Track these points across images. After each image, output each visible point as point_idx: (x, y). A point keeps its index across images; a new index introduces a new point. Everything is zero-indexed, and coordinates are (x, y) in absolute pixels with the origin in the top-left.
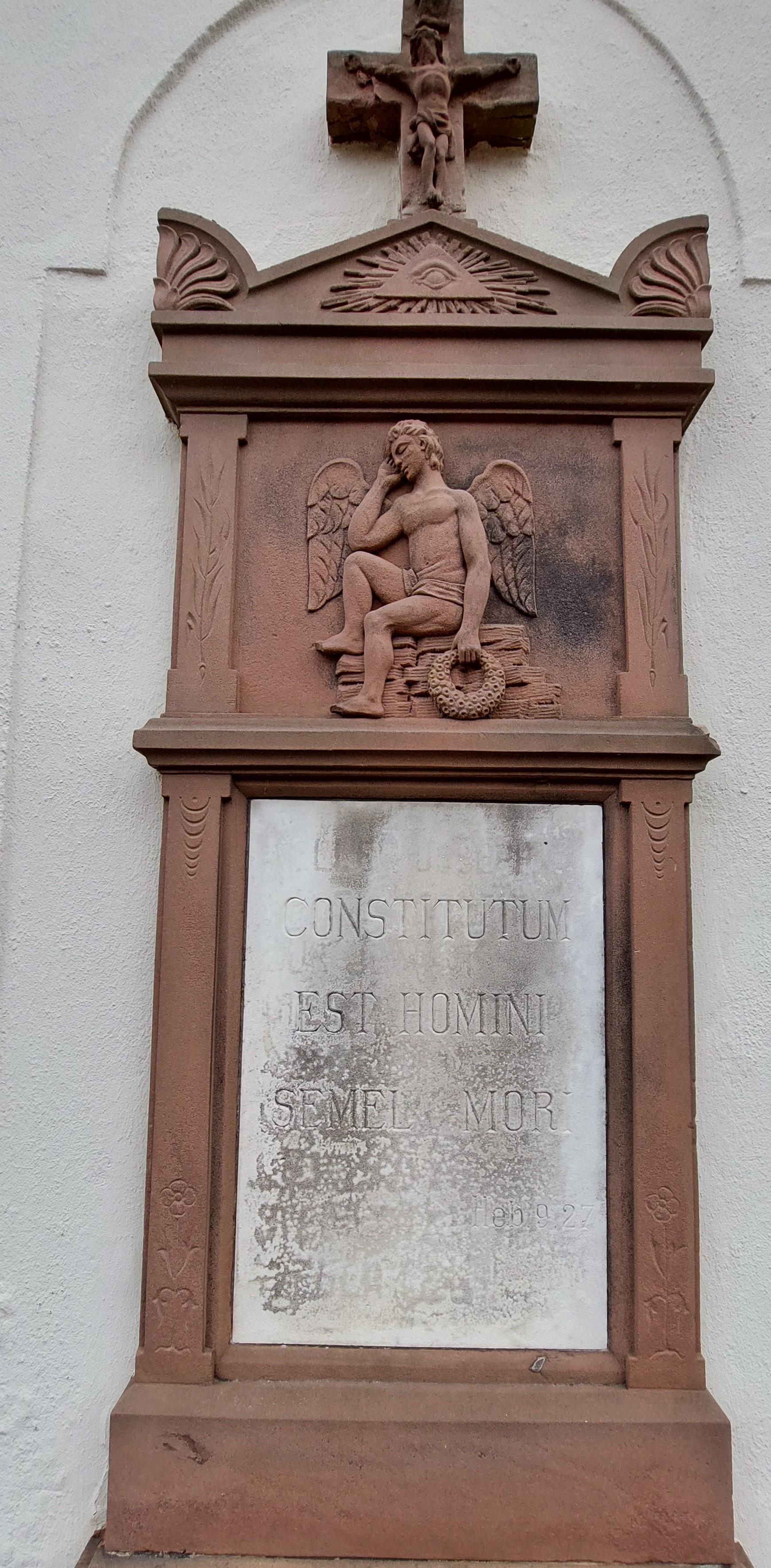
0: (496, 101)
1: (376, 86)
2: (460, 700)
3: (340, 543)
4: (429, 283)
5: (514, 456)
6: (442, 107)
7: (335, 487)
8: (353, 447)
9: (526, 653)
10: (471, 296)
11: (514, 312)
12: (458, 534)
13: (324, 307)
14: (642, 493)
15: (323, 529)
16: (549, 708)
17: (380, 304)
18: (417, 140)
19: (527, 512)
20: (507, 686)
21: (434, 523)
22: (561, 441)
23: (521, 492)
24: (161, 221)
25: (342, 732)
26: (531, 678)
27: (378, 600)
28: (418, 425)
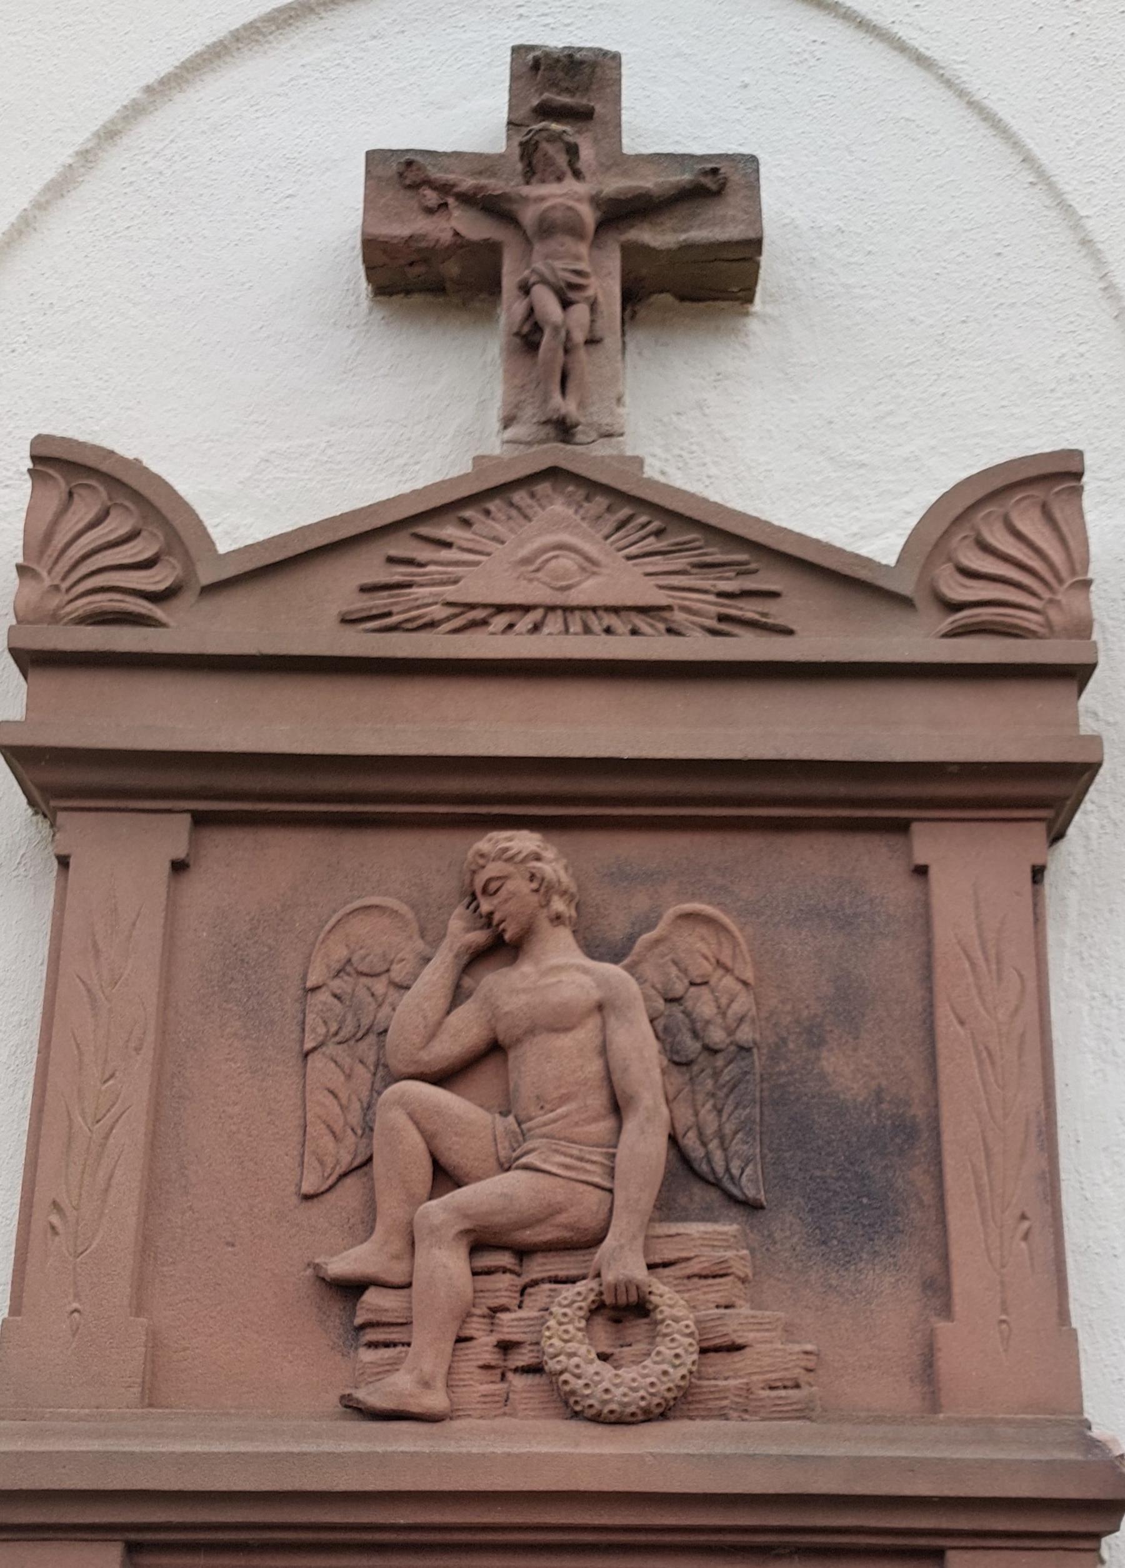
0: (683, 237)
1: (456, 213)
2: (605, 1385)
3: (371, 1059)
4: (548, 580)
6: (578, 258)
7: (362, 952)
8: (402, 868)
9: (744, 1280)
10: (629, 603)
11: (714, 632)
12: (604, 1050)
13: (347, 620)
14: (973, 965)
15: (336, 1034)
16: (794, 1398)
17: (456, 616)
18: (531, 311)
19: (743, 1003)
20: (703, 1351)
22: (812, 863)
23: (729, 962)
24: (34, 458)
25: (360, 1454)
26: (752, 1335)
27: (444, 1177)
28: (525, 841)
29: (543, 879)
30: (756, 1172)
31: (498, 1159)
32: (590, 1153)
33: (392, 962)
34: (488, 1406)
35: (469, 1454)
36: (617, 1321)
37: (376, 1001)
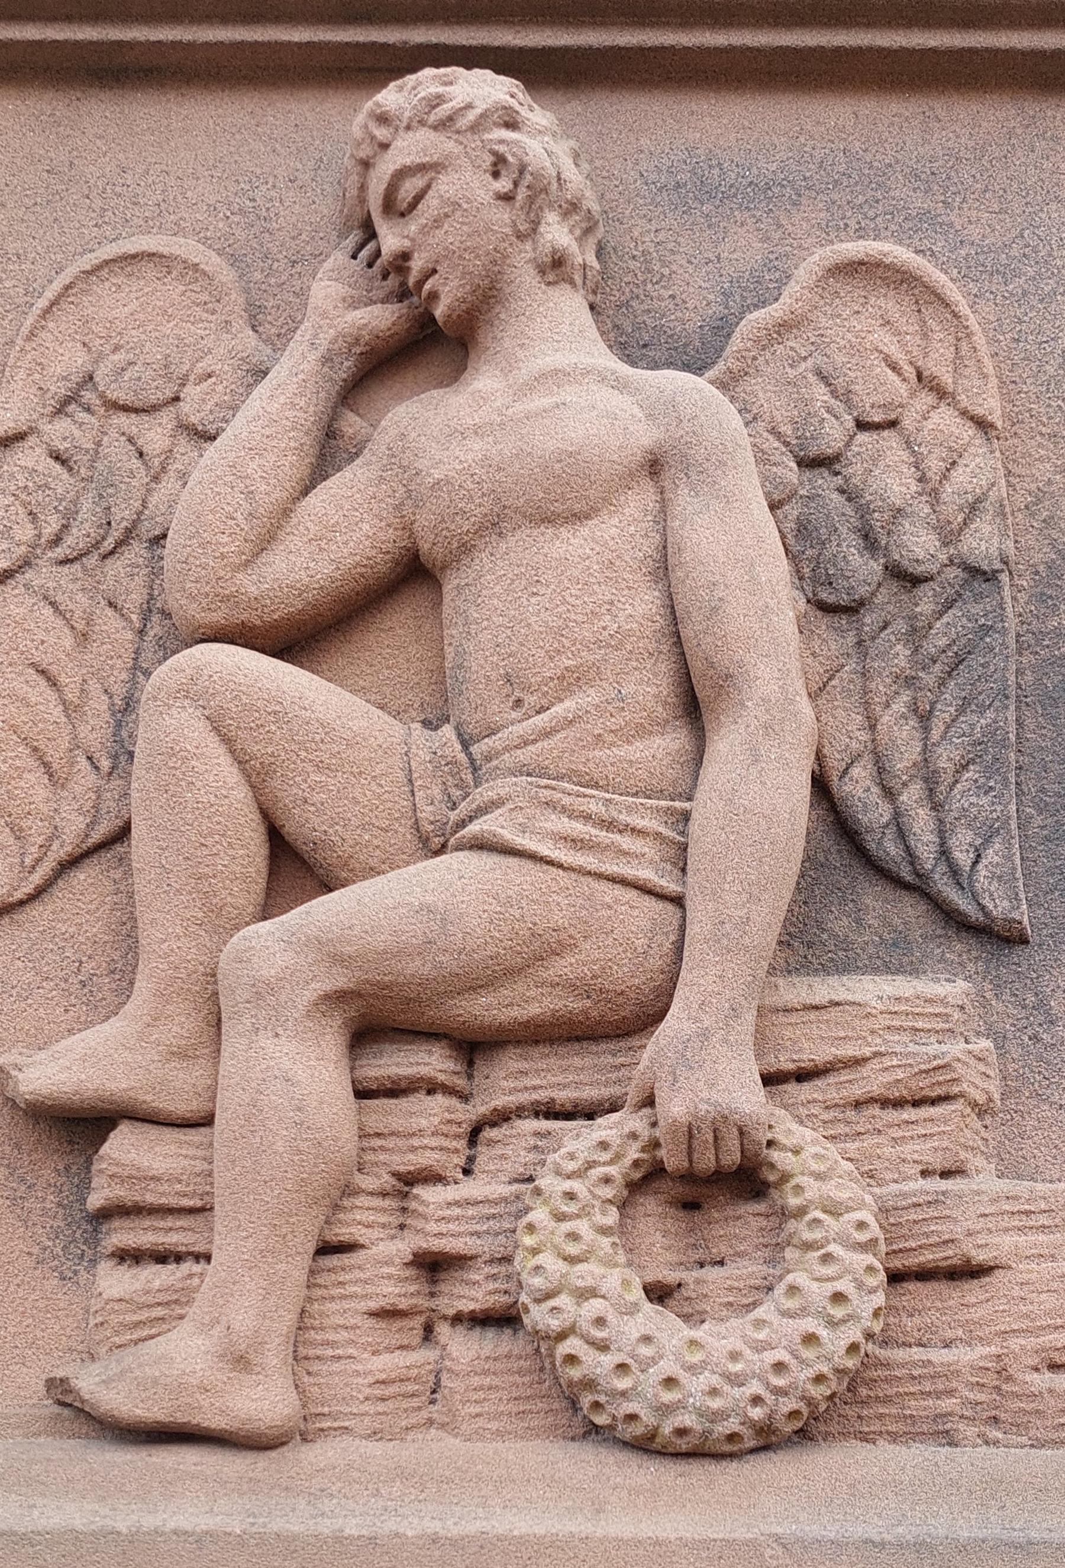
2: (667, 1367)
3: (134, 599)
5: (912, 226)
9: (982, 1110)
12: (663, 568)
15: (56, 541)
19: (978, 469)
20: (895, 1278)
21: (549, 519)
23: (947, 379)
26: (1008, 1241)
27: (293, 867)
28: (484, 89)
29: (522, 169)
30: (1009, 858)
31: (417, 826)
32: (629, 809)
33: (183, 382)
34: (390, 1405)
35: (339, 1539)
36: (691, 1206)
37: (148, 468)
